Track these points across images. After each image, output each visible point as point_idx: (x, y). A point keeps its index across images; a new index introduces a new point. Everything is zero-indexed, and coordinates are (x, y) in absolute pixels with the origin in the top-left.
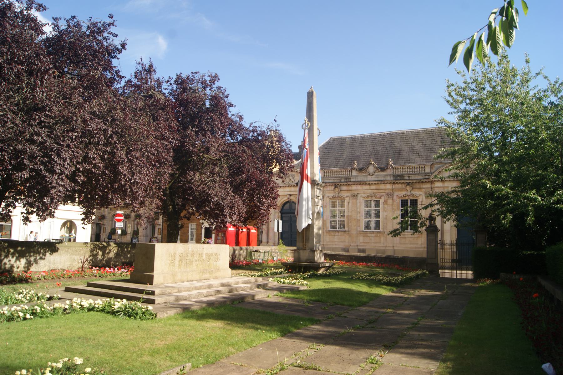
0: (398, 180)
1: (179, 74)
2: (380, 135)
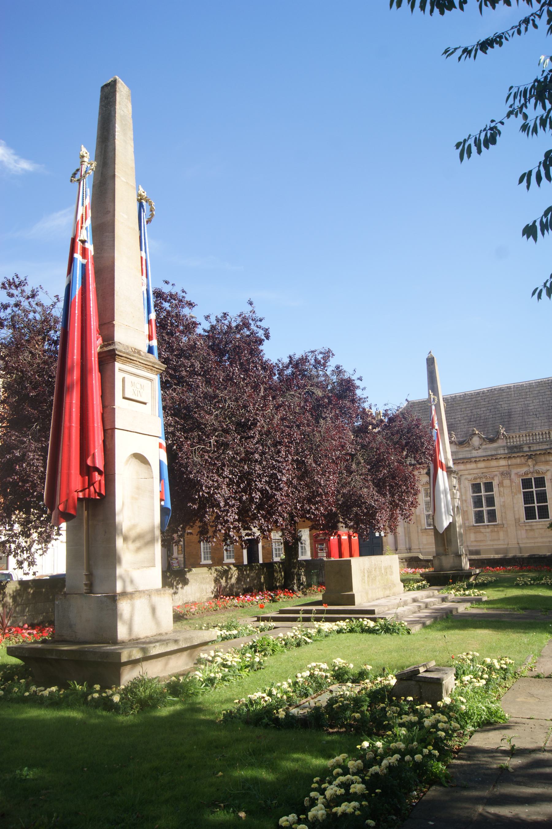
0: (515, 453)
1: (292, 354)
2: (478, 393)
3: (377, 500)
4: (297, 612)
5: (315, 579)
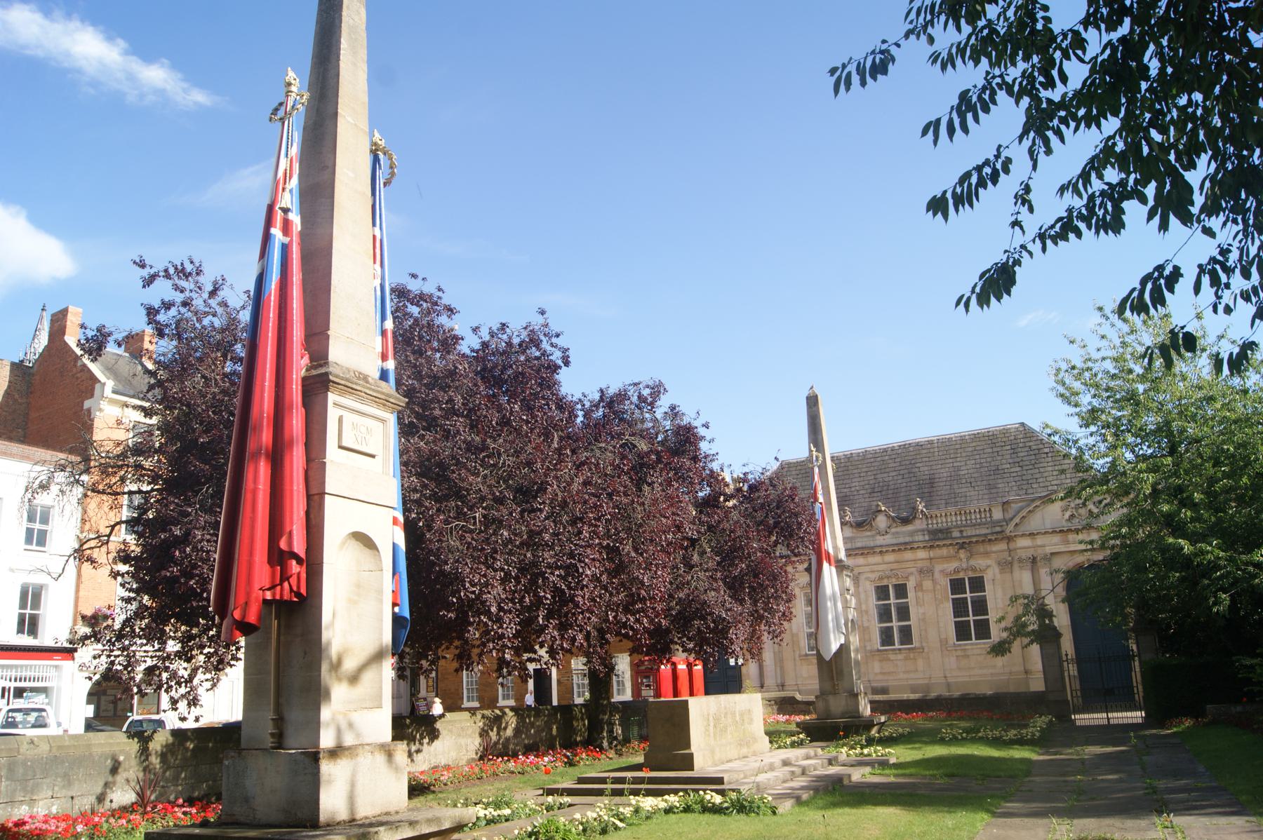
1: (603, 387)
2: (885, 450)
3: (730, 610)
4: (603, 781)
5: (635, 730)
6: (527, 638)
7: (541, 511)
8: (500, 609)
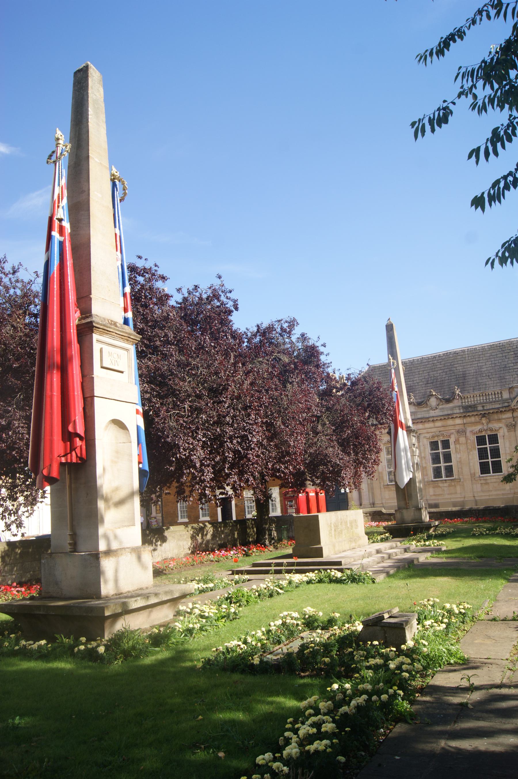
0: (469, 412)
1: (259, 323)
2: (435, 357)
3: (342, 459)
4: (269, 565)
5: (285, 533)
6: (219, 479)
7: (225, 402)
8: (202, 464)
